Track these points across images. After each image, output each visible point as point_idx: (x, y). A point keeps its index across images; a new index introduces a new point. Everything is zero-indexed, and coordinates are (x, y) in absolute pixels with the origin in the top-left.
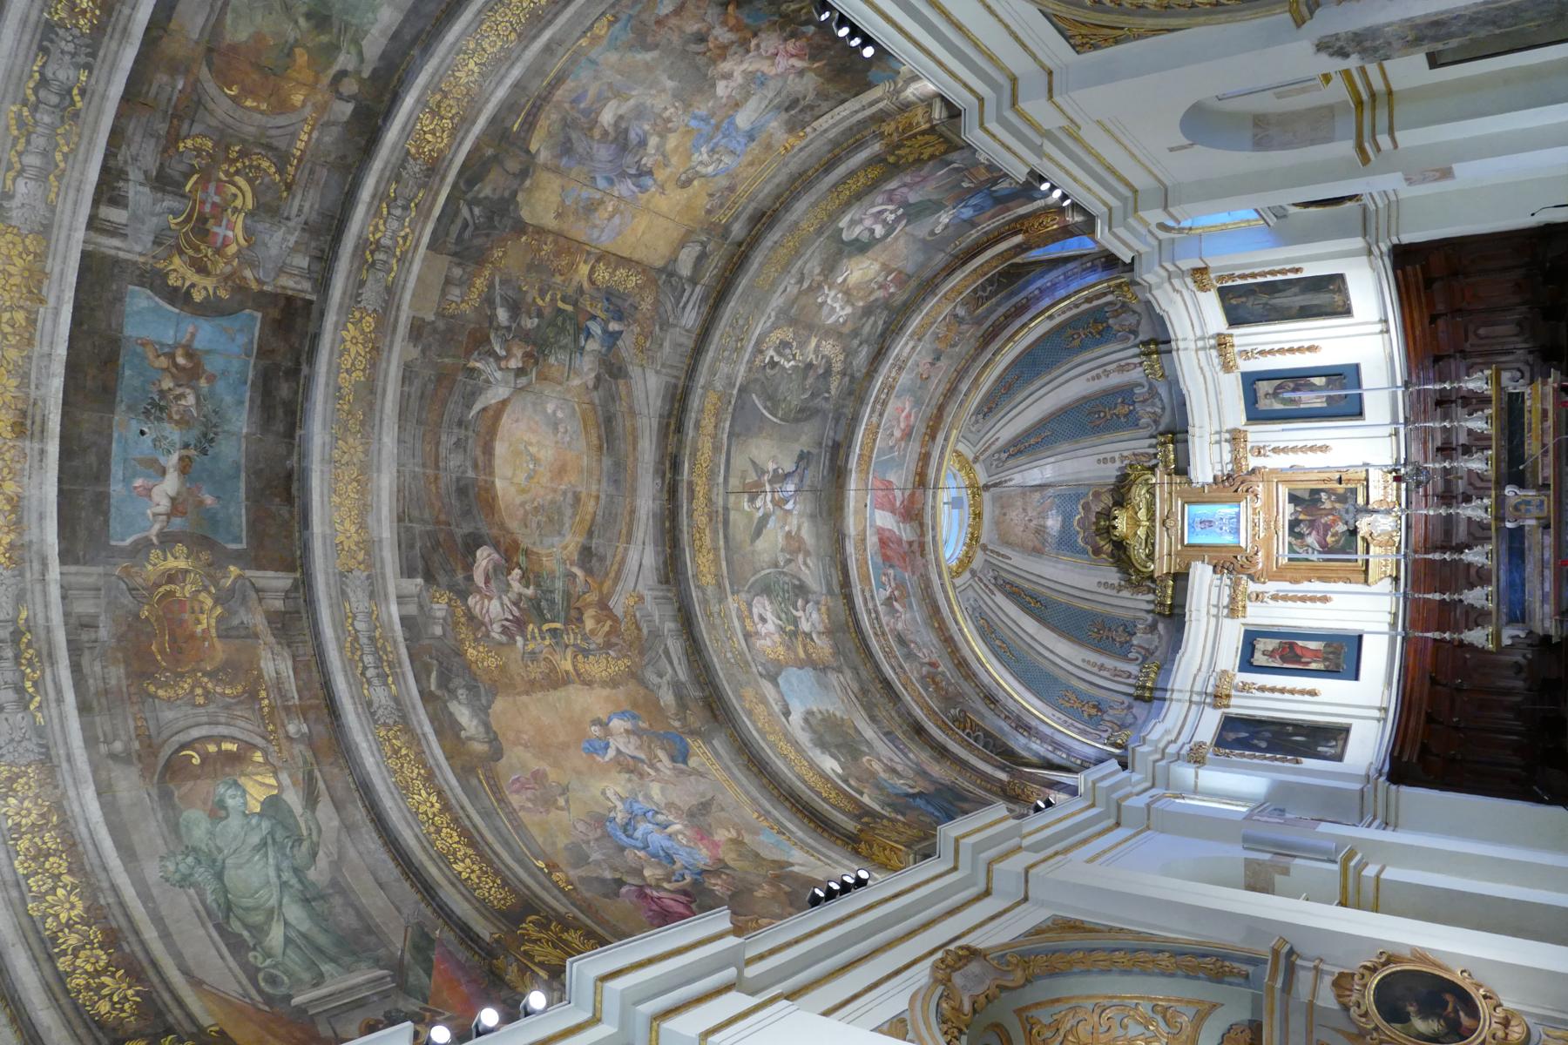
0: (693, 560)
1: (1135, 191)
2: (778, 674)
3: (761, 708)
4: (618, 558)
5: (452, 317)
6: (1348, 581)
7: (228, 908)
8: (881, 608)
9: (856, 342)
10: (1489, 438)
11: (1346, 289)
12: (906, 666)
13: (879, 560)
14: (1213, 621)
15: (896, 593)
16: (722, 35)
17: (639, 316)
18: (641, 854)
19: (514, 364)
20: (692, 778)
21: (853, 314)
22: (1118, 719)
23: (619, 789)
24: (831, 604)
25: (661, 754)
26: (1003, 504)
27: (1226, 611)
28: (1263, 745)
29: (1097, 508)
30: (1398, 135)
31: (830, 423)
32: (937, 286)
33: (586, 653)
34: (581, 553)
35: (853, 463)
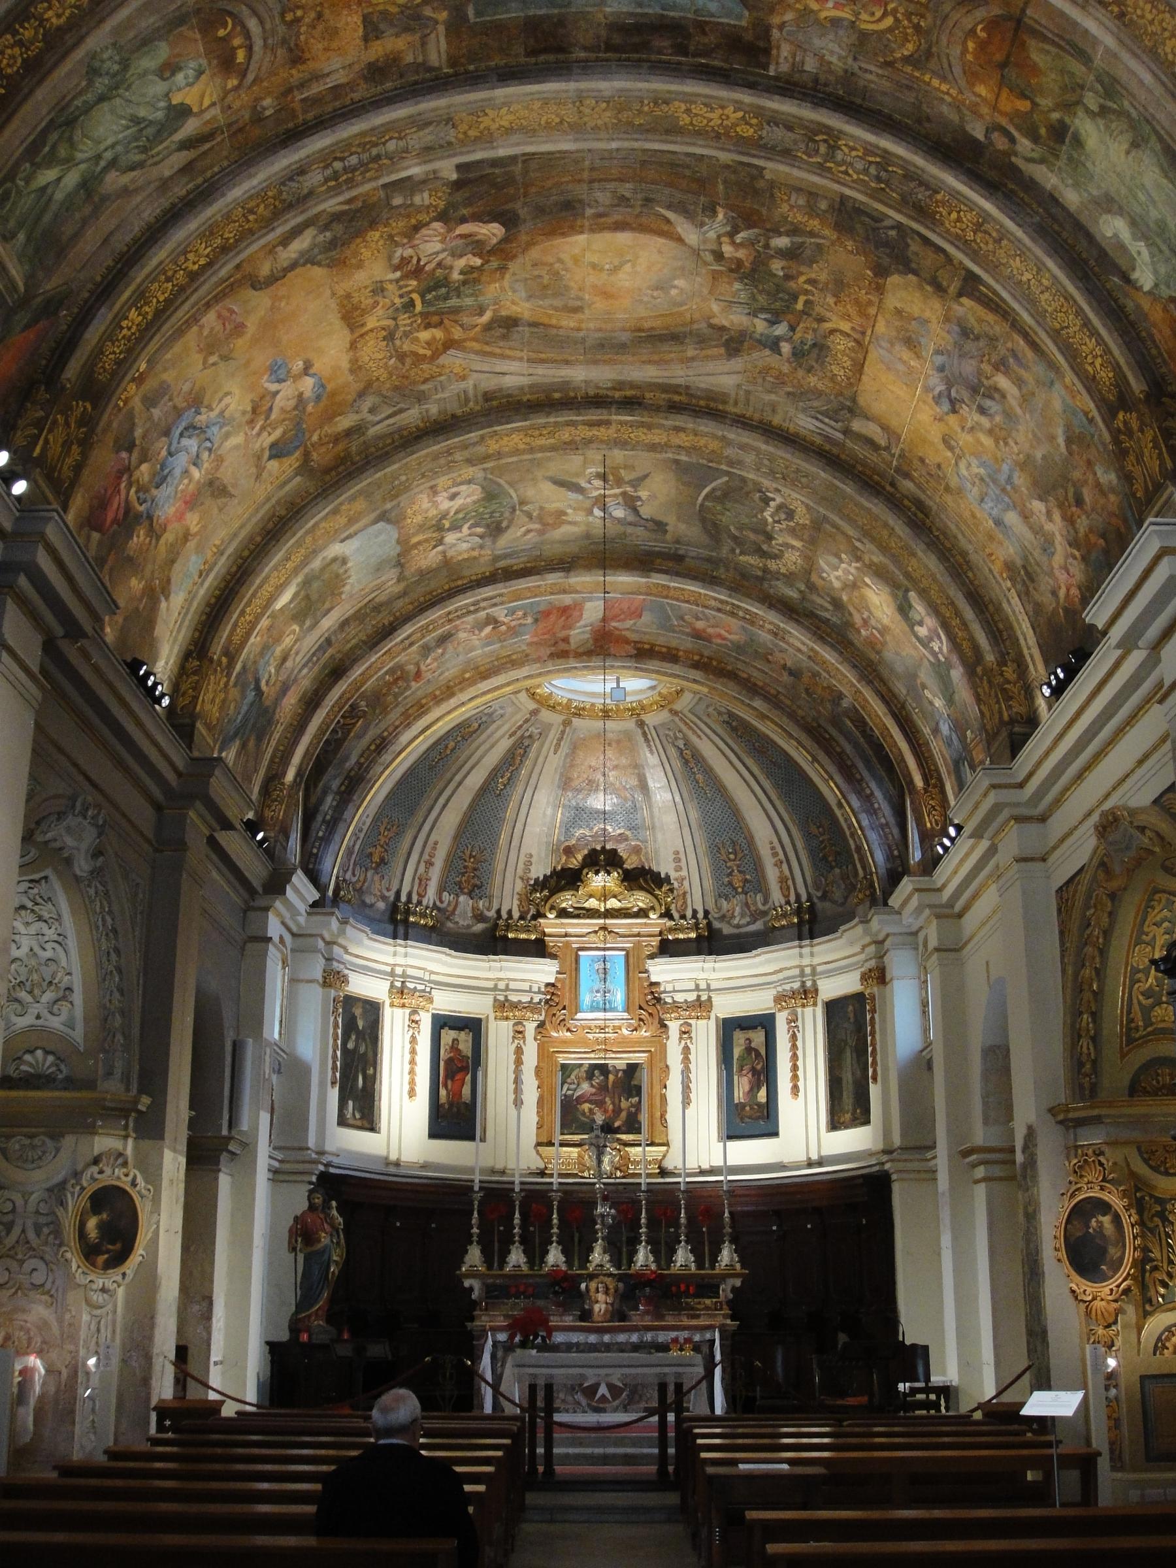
0: (518, 430)
1: (960, 915)
2: (389, 521)
3: (343, 520)
4: (508, 352)
5: (772, 196)
6: (540, 1126)
7: (71, 123)
8: (482, 614)
9: (803, 587)
10: (669, 1268)
11: (856, 1126)
12: (414, 648)
13: (542, 608)
14: (490, 984)
15: (504, 628)
16: (1083, 524)
17: (801, 373)
18: (164, 453)
19: (727, 249)
20: (254, 470)
21: (833, 589)
22: (369, 887)
23: (232, 407)
24: (482, 560)
25: (278, 433)
26: (624, 743)
27: (501, 998)
28: (350, 1045)
29: (622, 851)
30: (983, 1185)
31: (705, 553)
32: (870, 683)
33: (390, 337)
34: (508, 318)
35: (658, 579)
